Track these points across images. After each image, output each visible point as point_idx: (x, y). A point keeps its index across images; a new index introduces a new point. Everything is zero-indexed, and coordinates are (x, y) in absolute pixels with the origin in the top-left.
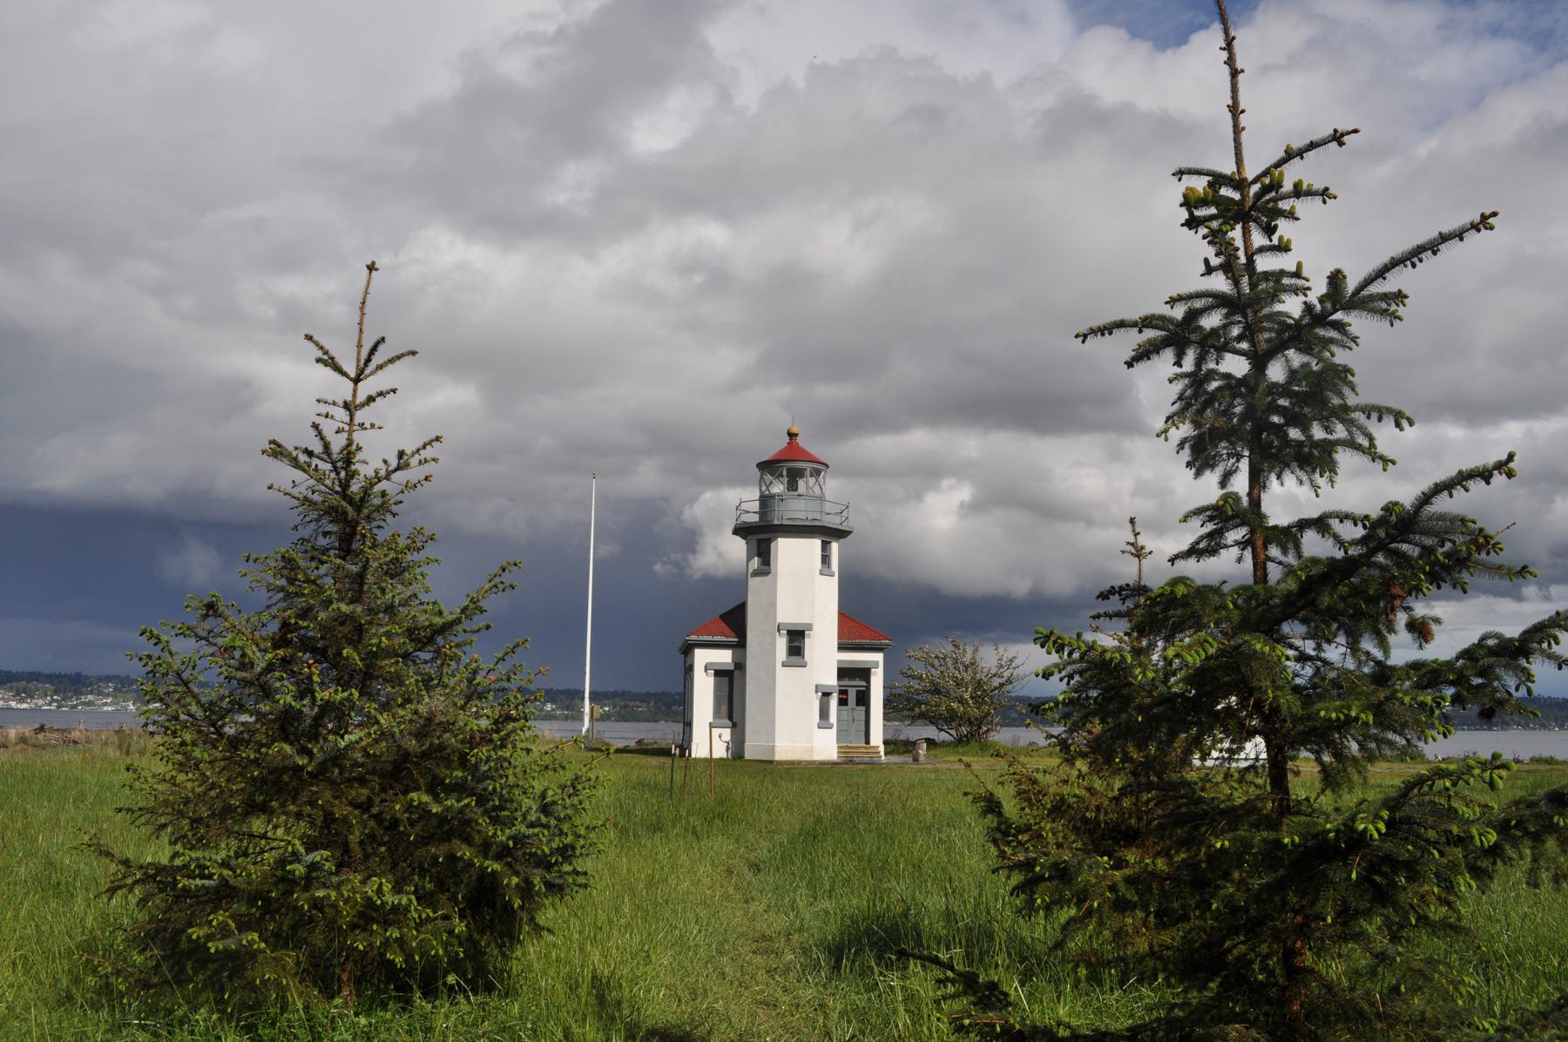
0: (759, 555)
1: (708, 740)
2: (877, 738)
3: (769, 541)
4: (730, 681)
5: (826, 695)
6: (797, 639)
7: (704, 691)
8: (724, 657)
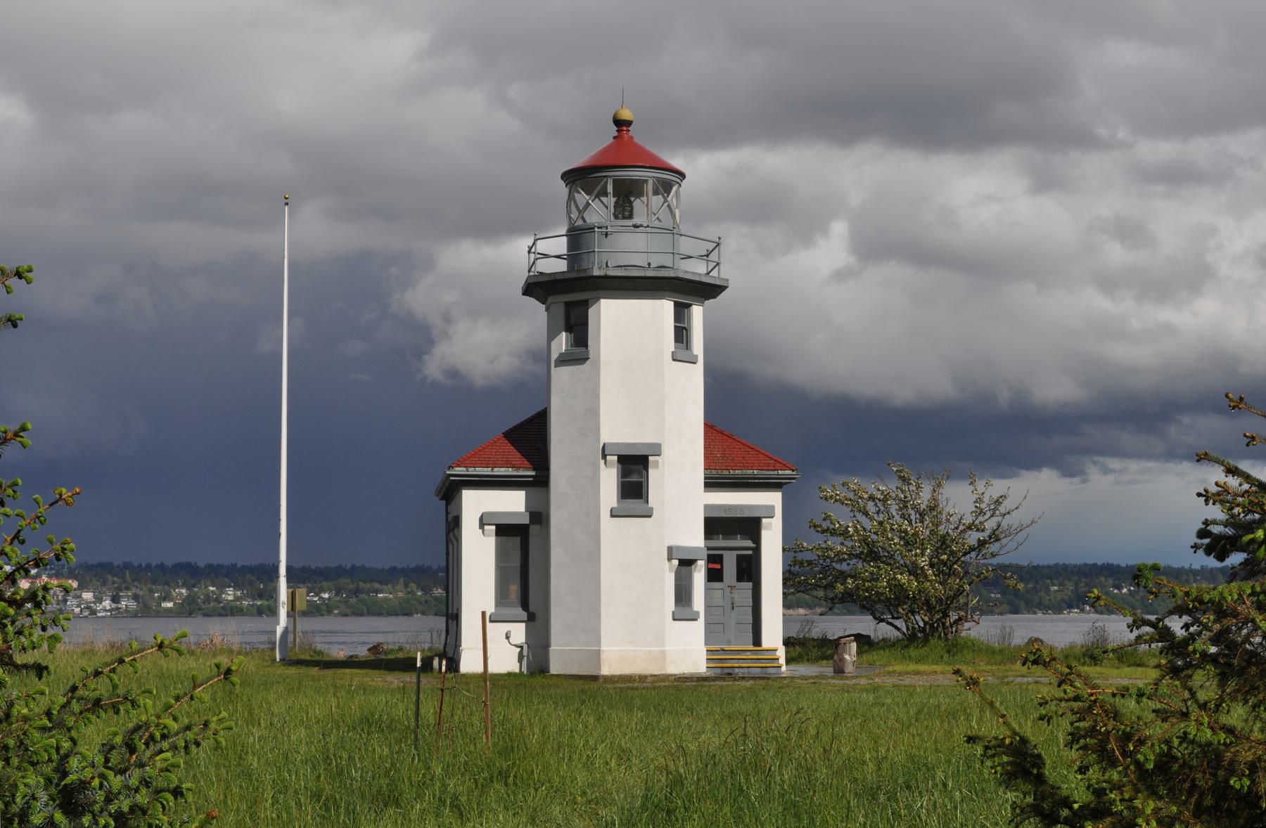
0: (569, 329)
1: (490, 645)
3: (585, 304)
4: (522, 542)
6: (634, 469)
7: (479, 559)
8: (512, 503)
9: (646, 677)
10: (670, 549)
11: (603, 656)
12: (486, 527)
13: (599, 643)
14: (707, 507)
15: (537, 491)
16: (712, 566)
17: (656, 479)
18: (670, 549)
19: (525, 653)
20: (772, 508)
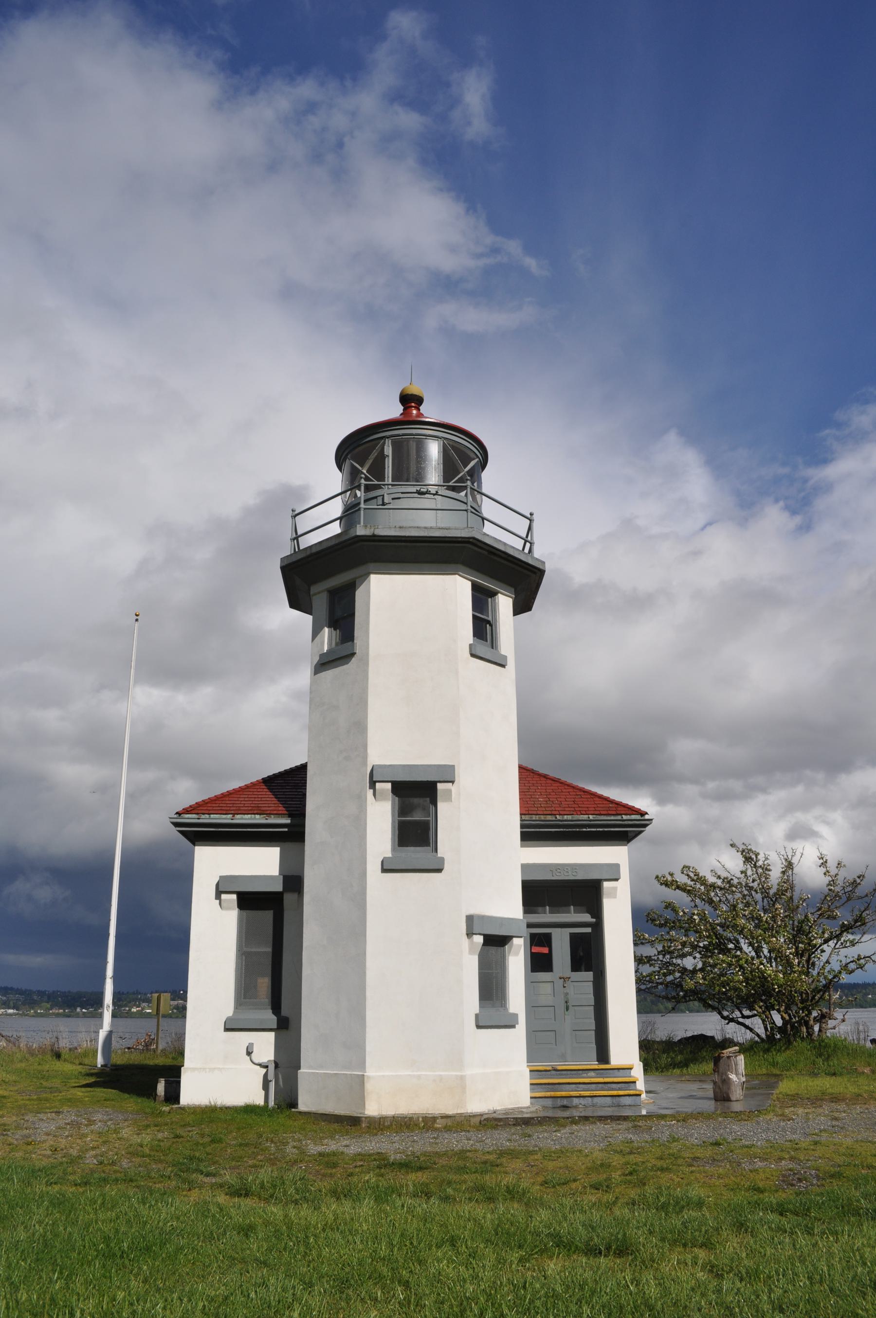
0: (333, 624)
1: (222, 1069)
2: (625, 1048)
3: (350, 589)
4: (270, 913)
5: (496, 942)
6: (416, 801)
7: (214, 939)
8: (261, 863)
9: (434, 1119)
10: (470, 919)
11: (368, 1086)
12: (224, 896)
13: (362, 1065)
14: (525, 867)
15: (289, 845)
16: (536, 949)
17: (451, 817)
18: (470, 919)
19: (271, 1076)
20: (616, 867)
